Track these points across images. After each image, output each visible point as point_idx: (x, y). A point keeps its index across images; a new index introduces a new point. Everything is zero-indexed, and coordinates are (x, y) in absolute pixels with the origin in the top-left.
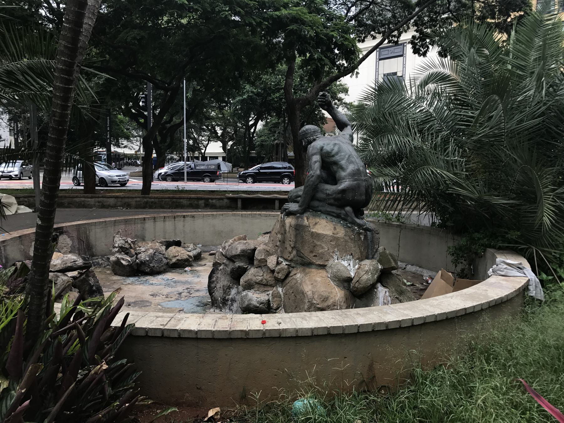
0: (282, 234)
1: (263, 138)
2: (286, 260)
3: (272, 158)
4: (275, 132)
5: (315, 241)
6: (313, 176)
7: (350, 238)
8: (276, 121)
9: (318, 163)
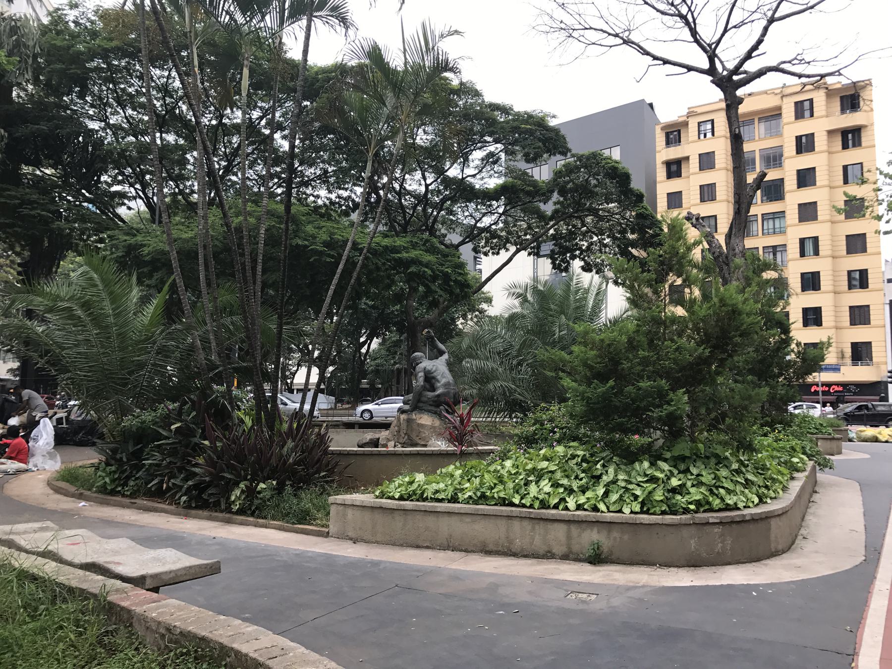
1: (378, 361)
3: (391, 389)
4: (396, 353)
8: (397, 337)
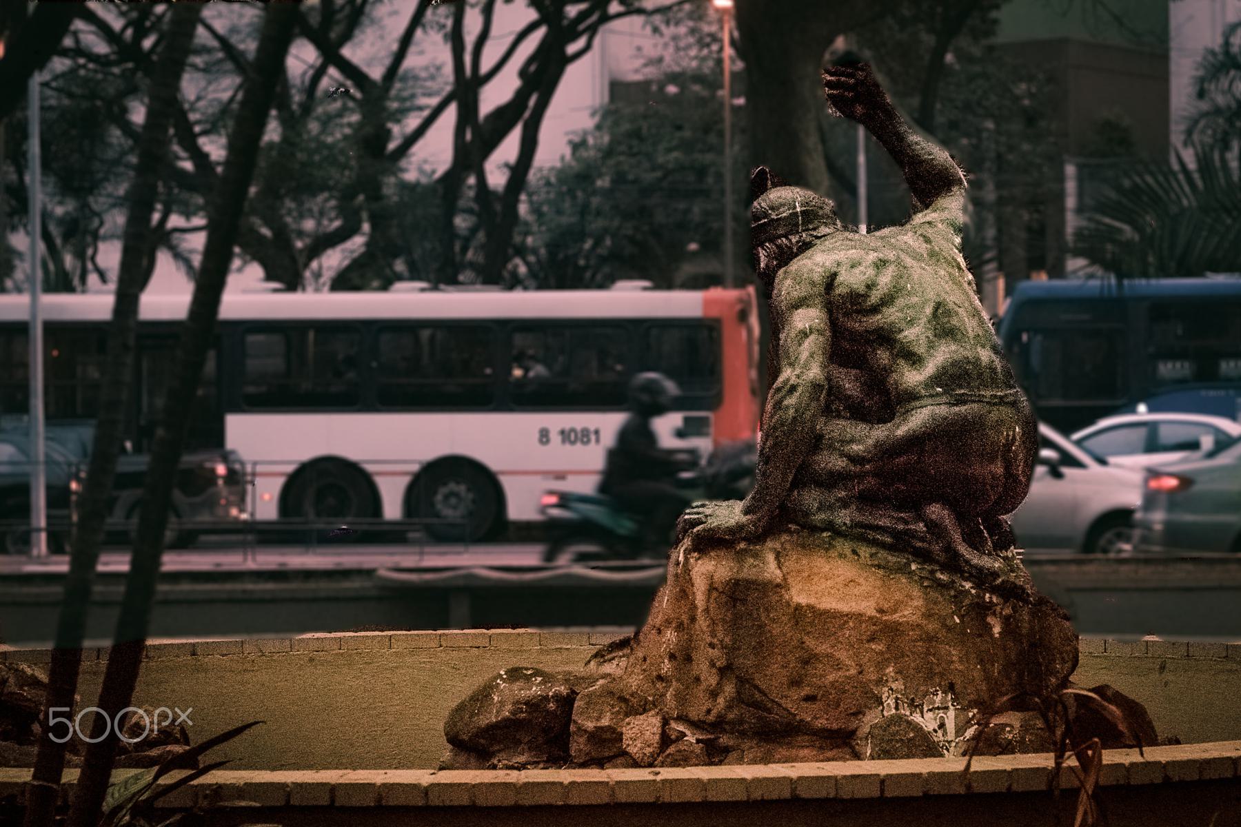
0: (680, 627)
2: (696, 725)
5: (810, 642)
6: (793, 388)
7: (944, 625)
9: (812, 337)
